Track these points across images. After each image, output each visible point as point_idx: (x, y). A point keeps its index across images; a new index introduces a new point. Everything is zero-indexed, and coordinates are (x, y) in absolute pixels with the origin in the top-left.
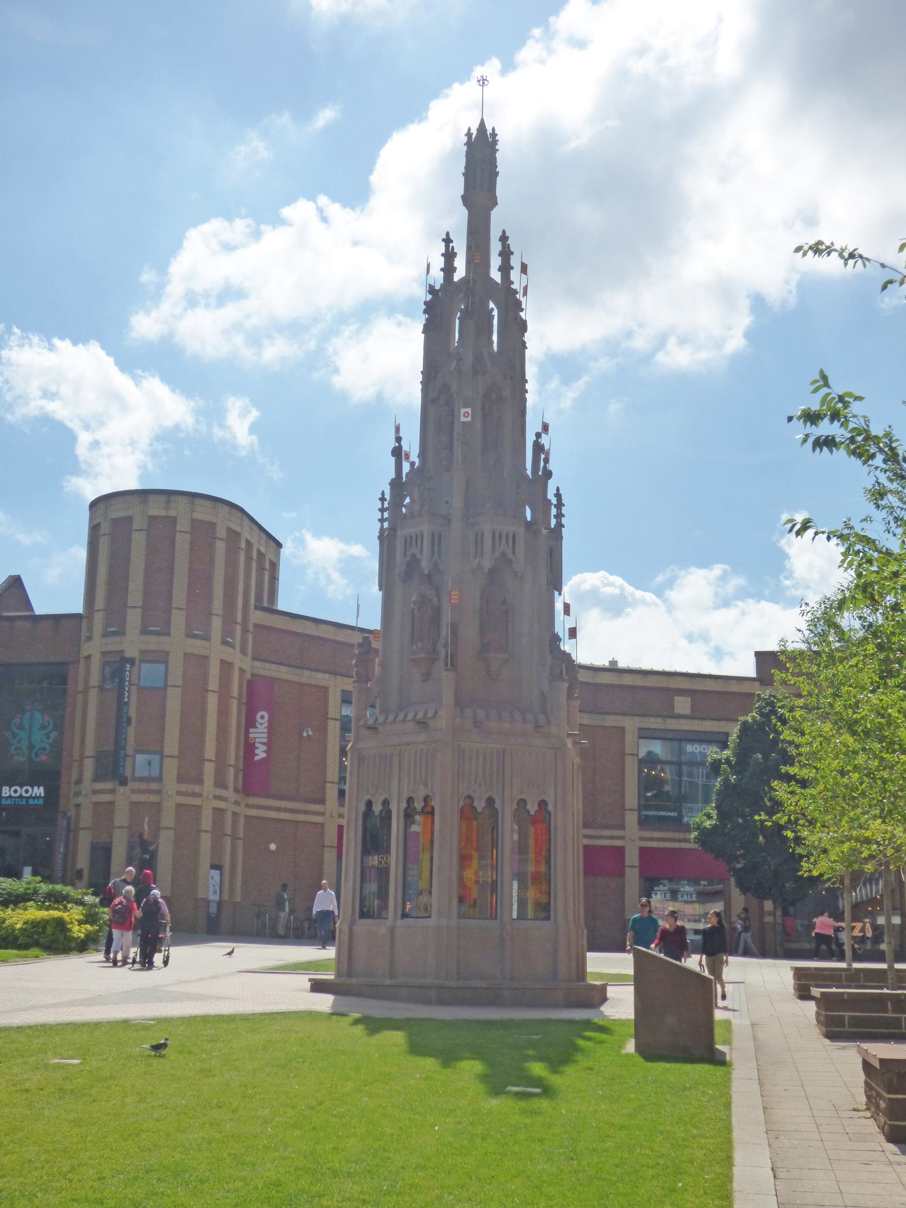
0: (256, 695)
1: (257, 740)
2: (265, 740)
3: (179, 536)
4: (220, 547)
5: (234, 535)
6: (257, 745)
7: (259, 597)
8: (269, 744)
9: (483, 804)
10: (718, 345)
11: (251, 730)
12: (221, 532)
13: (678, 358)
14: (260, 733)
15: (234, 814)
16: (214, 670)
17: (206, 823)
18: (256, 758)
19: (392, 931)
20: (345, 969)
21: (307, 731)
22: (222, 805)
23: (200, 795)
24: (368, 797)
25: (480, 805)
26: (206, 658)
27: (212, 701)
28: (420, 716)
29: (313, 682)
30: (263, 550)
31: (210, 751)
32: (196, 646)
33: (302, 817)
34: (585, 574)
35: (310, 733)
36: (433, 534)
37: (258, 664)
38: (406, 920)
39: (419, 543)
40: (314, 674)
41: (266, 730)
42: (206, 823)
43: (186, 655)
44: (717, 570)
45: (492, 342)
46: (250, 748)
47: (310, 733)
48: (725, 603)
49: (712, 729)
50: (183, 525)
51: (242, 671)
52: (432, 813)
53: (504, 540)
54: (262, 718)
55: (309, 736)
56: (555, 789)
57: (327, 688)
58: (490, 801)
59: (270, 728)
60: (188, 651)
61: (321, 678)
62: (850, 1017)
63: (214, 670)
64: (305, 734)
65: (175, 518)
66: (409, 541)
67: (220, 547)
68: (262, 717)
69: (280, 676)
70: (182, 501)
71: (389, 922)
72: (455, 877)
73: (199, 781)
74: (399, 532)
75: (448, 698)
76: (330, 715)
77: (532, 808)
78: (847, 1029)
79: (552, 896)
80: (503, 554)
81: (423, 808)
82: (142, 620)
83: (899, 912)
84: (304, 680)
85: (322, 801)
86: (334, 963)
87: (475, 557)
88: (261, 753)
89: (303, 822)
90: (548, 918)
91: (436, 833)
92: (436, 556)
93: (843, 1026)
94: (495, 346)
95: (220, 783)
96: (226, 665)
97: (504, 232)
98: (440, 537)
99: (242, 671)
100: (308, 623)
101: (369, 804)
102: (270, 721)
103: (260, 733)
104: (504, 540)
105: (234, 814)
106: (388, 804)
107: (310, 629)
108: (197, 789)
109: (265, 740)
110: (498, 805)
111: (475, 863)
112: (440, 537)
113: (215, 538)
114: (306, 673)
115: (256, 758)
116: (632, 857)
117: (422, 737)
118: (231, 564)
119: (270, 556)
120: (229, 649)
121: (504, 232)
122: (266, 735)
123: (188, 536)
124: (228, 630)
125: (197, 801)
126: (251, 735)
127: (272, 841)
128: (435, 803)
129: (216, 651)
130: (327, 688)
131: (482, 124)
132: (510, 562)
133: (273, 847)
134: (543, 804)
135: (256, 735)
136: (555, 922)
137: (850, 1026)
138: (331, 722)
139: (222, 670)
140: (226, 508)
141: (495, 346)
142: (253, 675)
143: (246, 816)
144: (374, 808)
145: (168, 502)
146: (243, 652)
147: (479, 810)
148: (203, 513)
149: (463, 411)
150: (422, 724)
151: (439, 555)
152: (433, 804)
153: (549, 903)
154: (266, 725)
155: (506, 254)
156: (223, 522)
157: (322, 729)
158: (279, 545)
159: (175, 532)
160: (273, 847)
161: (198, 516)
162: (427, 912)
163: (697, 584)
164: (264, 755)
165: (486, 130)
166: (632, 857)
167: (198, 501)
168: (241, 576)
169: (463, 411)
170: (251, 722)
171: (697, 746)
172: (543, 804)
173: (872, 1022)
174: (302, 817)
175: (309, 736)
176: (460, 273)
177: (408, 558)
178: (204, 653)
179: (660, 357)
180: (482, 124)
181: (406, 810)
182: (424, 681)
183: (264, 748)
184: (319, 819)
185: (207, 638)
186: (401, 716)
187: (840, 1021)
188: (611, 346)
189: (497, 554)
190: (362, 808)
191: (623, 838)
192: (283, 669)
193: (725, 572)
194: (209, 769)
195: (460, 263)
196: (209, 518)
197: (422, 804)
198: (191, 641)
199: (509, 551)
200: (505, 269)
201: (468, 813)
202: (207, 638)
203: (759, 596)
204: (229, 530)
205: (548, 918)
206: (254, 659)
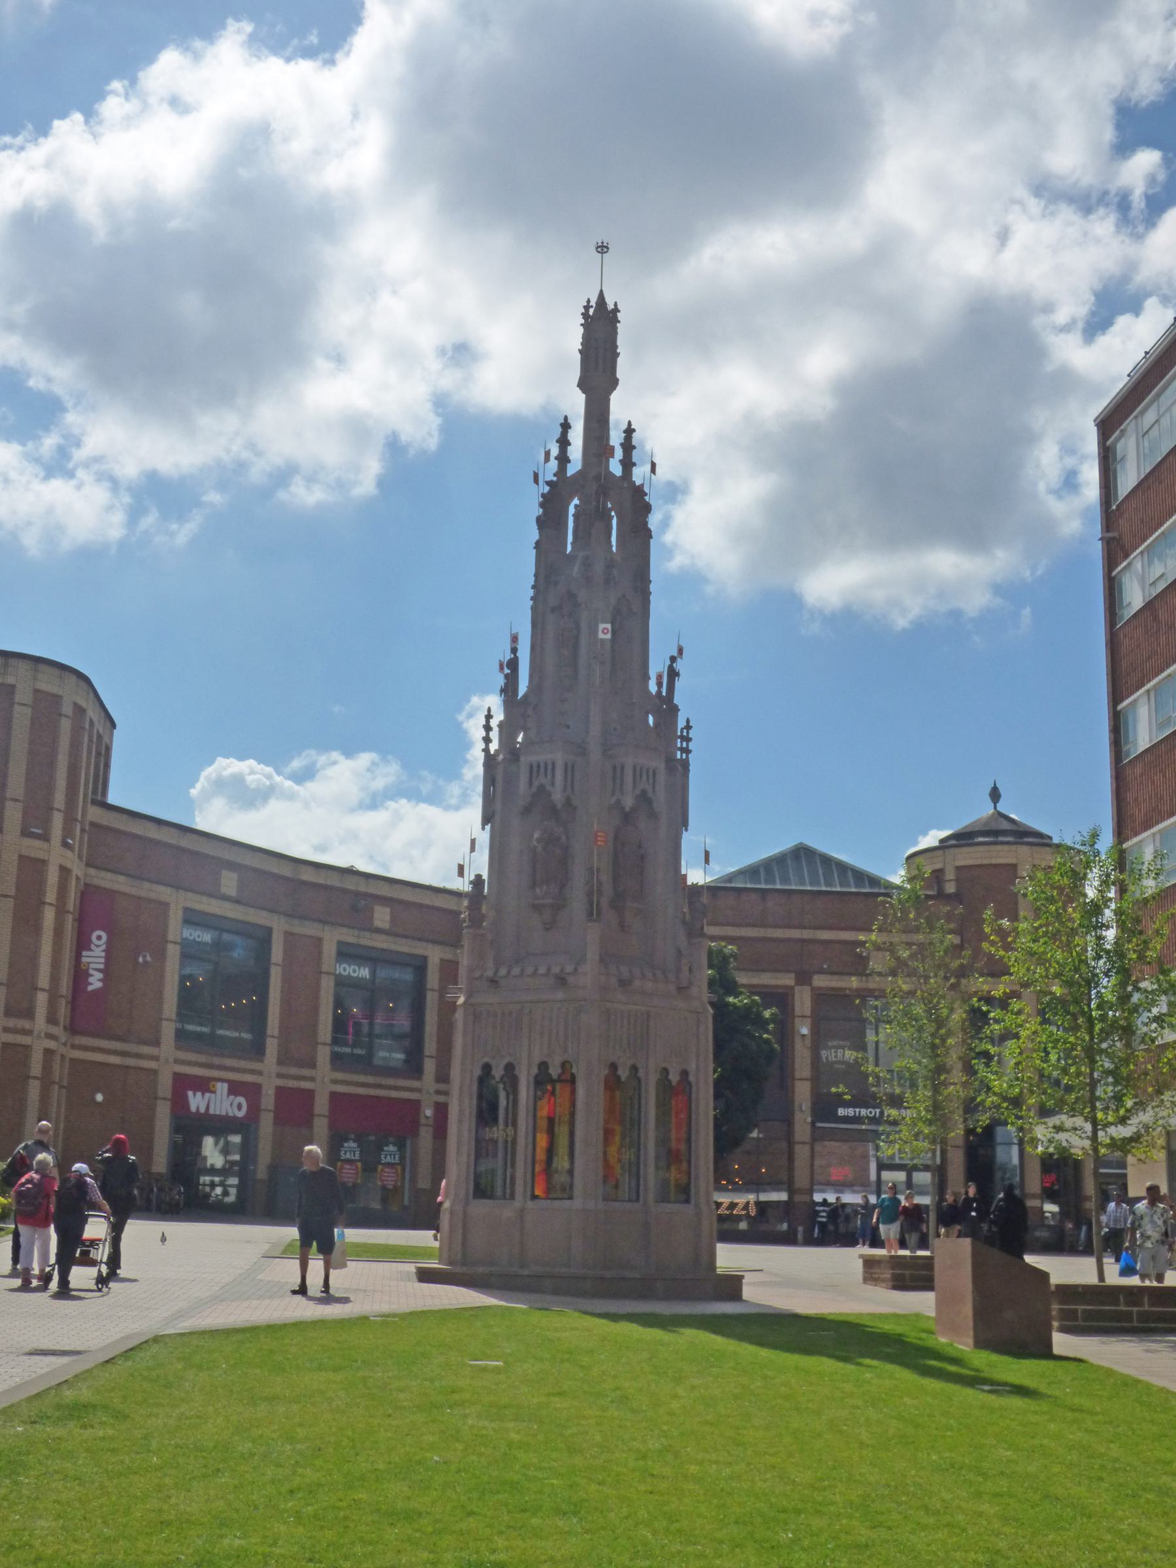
0: (93, 910)
1: (92, 966)
2: (102, 966)
3: (17, 709)
4: (66, 725)
5: (80, 711)
6: (91, 972)
7: (95, 791)
8: (107, 971)
9: (627, 1073)
10: (341, 485)
11: (84, 953)
12: (67, 709)
13: (307, 496)
14: (95, 957)
15: (62, 1056)
16: (52, 877)
17: (36, 1069)
18: (90, 988)
19: (522, 1212)
20: (459, 1256)
21: (145, 956)
22: (52, 1045)
23: (29, 1033)
24: (486, 1060)
25: (623, 1073)
26: (44, 862)
27: (49, 915)
28: (556, 970)
29: (153, 896)
30: (101, 731)
31: (44, 980)
32: (34, 848)
33: (131, 1062)
34: (232, 760)
35: (149, 959)
36: (566, 764)
37: (92, 871)
38: (536, 1201)
39: (549, 772)
40: (154, 886)
41: (103, 954)
42: (36, 1069)
43: (21, 857)
44: (365, 759)
45: (611, 546)
46: (80, 975)
47: (149, 959)
48: (374, 802)
49: (281, 948)
50: (23, 695)
51: (78, 878)
52: (573, 1081)
53: (645, 777)
54: (99, 939)
55: (145, 962)
56: (698, 1057)
57: (167, 905)
58: (634, 1068)
59: (108, 951)
60: (25, 852)
61: (163, 893)
62: (1084, 1311)
63: (52, 877)
64: (141, 960)
65: (13, 687)
66: (533, 770)
67: (66, 725)
68: (99, 938)
69: (117, 887)
70: (23, 666)
71: (517, 1203)
72: (601, 1155)
73: (30, 1014)
74: (522, 759)
75: (593, 954)
76: (171, 937)
77: (674, 1078)
78: (1135, 1324)
79: (693, 1177)
80: (644, 792)
81: (560, 1076)
82: (23, 817)
83: (786, 1186)
84: (143, 894)
85: (157, 1043)
86: (298, 1243)
87: (613, 793)
88: (95, 982)
89: (134, 1068)
90: (687, 1201)
91: (580, 1105)
92: (569, 788)
93: (1076, 1319)
94: (614, 549)
95: (52, 1019)
96: (64, 871)
97: (630, 423)
98: (573, 767)
99: (78, 878)
100: (149, 825)
101: (487, 1068)
102: (109, 943)
103: (95, 957)
104: (645, 777)
105: (62, 1056)
106: (514, 1068)
107: (153, 832)
108: (26, 1024)
109: (102, 966)
110: (641, 1074)
111: (617, 1138)
112: (573, 767)
113: (60, 715)
114: (147, 885)
115: (90, 988)
116: (322, 1105)
117: (560, 995)
118: (75, 746)
119: (106, 739)
120: (69, 853)
121: (630, 423)
122: (103, 960)
123: (29, 711)
124: (67, 832)
125: (25, 1040)
126: (84, 960)
127: (99, 1090)
128: (579, 1071)
129: (56, 855)
130: (167, 905)
131: (601, 296)
132: (649, 802)
133: (99, 1097)
134: (684, 1073)
135: (89, 960)
136: (697, 1206)
137: (1139, 1321)
138: (170, 947)
139: (60, 877)
140: (74, 678)
141: (614, 549)
142: (86, 885)
143: (71, 1059)
144: (493, 1072)
145: (6, 665)
146: (80, 857)
147: (623, 1078)
148: (48, 683)
149: (602, 626)
150: (561, 981)
151: (572, 788)
152: (574, 1071)
153: (689, 1184)
154: (103, 947)
155: (628, 446)
156: (71, 694)
157: (161, 955)
158: (114, 726)
159: (12, 705)
160: (99, 1097)
161: (43, 686)
162: (567, 1192)
163: (344, 774)
164: (99, 985)
165: (605, 304)
166: (322, 1105)
167: (42, 667)
168: (84, 764)
169: (602, 626)
170: (83, 943)
171: (352, 974)
172: (684, 1073)
173: (1100, 1316)
174: (131, 1062)
175: (145, 962)
176: (576, 463)
177: (534, 789)
178: (41, 855)
179: (282, 495)
180: (601, 296)
181: (536, 1076)
182: (547, 929)
183: (100, 975)
184: (152, 1065)
185: (45, 837)
186: (516, 971)
187: (1072, 1315)
188: (229, 474)
189: (638, 791)
190: (478, 1072)
191: (419, 1090)
192: (121, 878)
193: (374, 764)
194: (42, 999)
195: (576, 451)
196: (54, 690)
197: (560, 1071)
198: (27, 841)
199: (649, 789)
200: (628, 464)
201: (613, 1082)
202: (45, 837)
203: (415, 796)
204: (75, 704)
205: (687, 1201)
206: (88, 865)
